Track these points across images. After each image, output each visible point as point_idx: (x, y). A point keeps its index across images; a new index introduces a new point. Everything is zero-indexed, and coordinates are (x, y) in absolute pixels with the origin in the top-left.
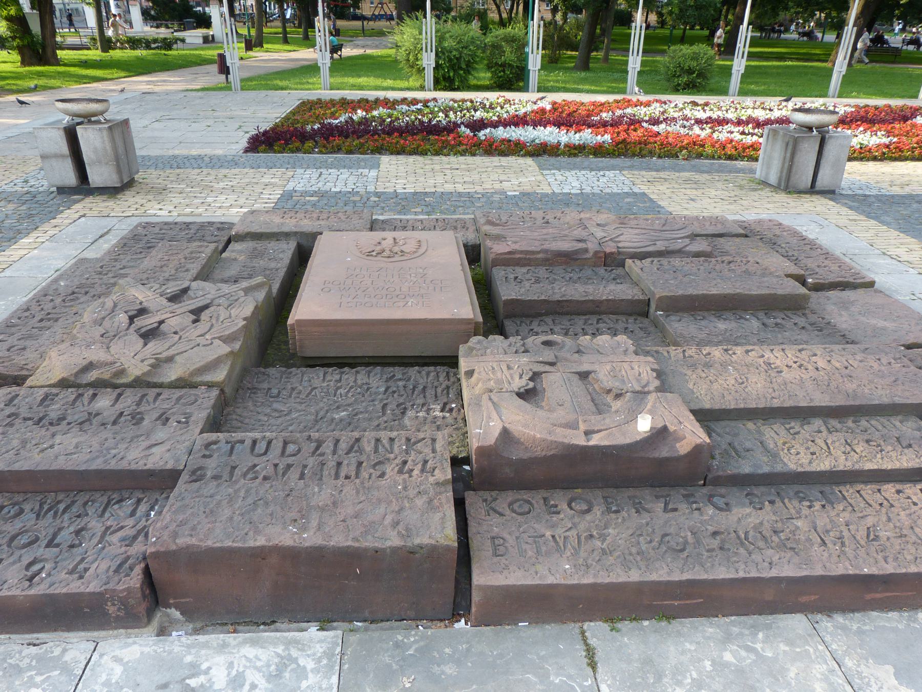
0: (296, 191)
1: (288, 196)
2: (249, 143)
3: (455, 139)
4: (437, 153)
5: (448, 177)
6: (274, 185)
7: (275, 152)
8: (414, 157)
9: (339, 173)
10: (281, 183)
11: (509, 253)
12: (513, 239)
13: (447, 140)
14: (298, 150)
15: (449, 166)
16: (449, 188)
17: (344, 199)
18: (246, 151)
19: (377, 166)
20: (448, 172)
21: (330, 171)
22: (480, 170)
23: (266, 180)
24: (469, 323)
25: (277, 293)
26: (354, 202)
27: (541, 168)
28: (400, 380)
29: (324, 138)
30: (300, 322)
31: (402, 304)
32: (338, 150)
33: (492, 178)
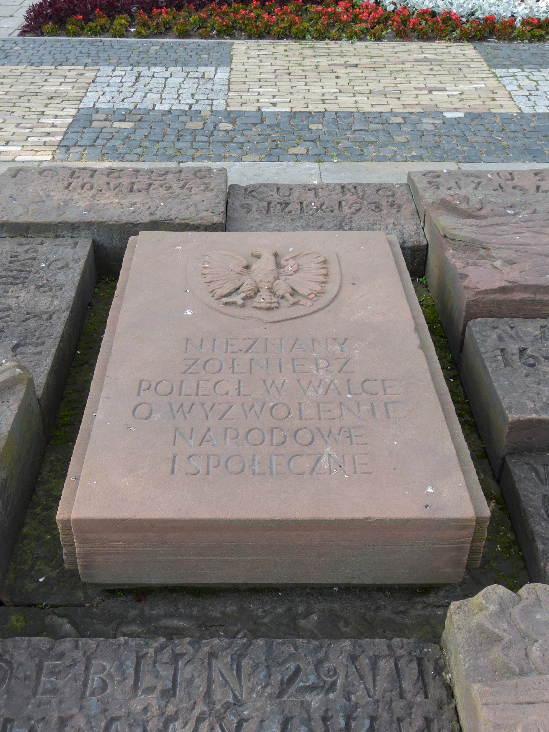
0: (97, 111)
1: (84, 120)
2: (27, 19)
3: (347, 10)
4: (321, 36)
5: (343, 82)
6: (63, 98)
7: (68, 34)
8: (285, 42)
9: (167, 74)
10: (73, 93)
11: (503, 290)
12: (504, 254)
13: (335, 13)
14: (103, 31)
15: (341, 61)
16: (346, 103)
17: (178, 125)
18: (23, 33)
19: (227, 60)
20: (341, 71)
21: (153, 69)
22: (393, 67)
23: (50, 88)
24: (464, 527)
25: (48, 385)
26: (193, 132)
27: (492, 63)
28: (312, 688)
29: (145, 10)
30: (85, 525)
31: (305, 463)
32: (164, 30)
33: (414, 84)
